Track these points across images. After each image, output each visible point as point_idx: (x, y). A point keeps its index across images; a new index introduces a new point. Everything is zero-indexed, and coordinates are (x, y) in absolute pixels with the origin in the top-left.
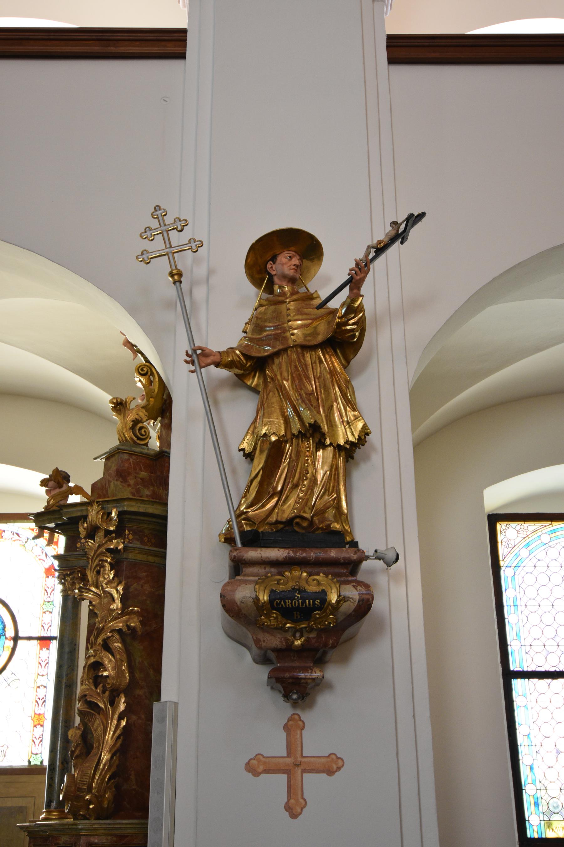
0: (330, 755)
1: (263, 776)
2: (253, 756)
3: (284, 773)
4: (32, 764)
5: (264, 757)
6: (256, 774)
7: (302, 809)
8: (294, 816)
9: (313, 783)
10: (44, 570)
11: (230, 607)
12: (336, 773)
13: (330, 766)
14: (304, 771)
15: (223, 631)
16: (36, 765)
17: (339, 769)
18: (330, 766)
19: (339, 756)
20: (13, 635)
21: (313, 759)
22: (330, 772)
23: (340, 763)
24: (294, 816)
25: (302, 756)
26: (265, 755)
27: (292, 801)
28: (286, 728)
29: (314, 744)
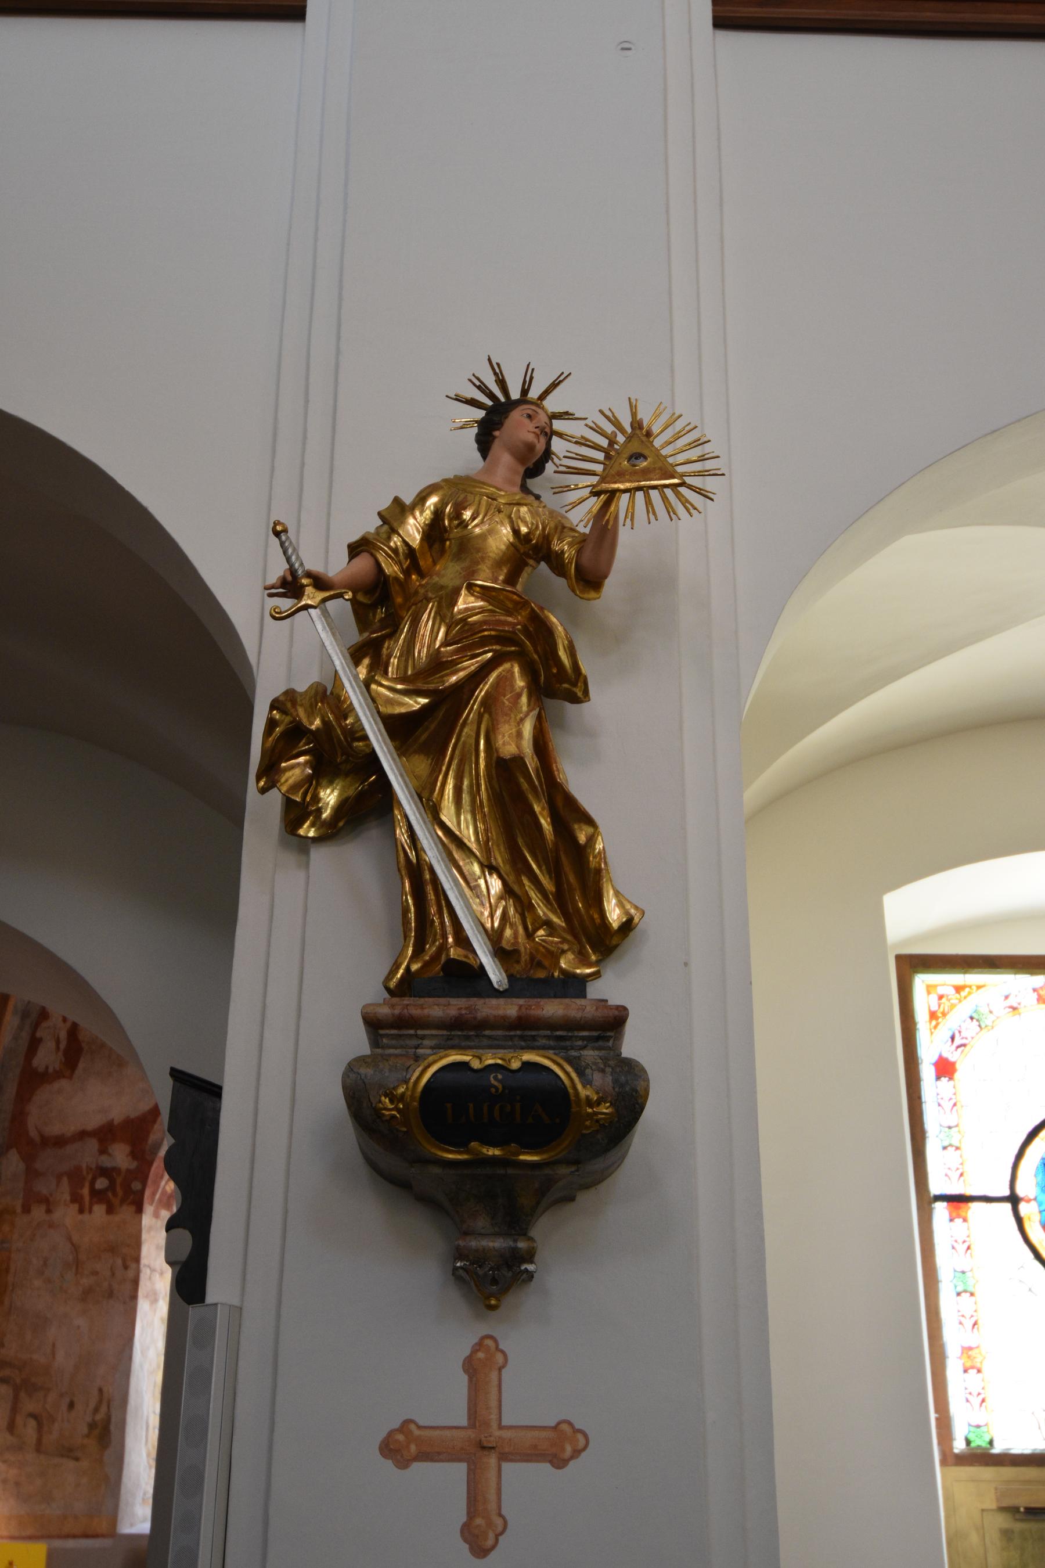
0: (559, 1423)
1: (416, 1466)
2: (396, 1425)
3: (460, 1460)
4: (973, 1445)
5: (419, 1427)
6: (403, 1463)
7: (497, 1536)
8: (480, 1551)
9: (521, 1483)
10: (956, 1076)
11: (359, 1097)
12: (572, 1463)
13: (558, 1446)
14: (504, 1457)
15: (360, 1155)
16: (979, 1447)
17: (577, 1453)
18: (558, 1446)
19: (577, 1427)
20: (1023, 1207)
21: (448, 1433)
22: (559, 1463)
23: (582, 1441)
24: (480, 1551)
25: (501, 1427)
26: (421, 1423)
27: (479, 1521)
28: (471, 1367)
29: (525, 1401)
